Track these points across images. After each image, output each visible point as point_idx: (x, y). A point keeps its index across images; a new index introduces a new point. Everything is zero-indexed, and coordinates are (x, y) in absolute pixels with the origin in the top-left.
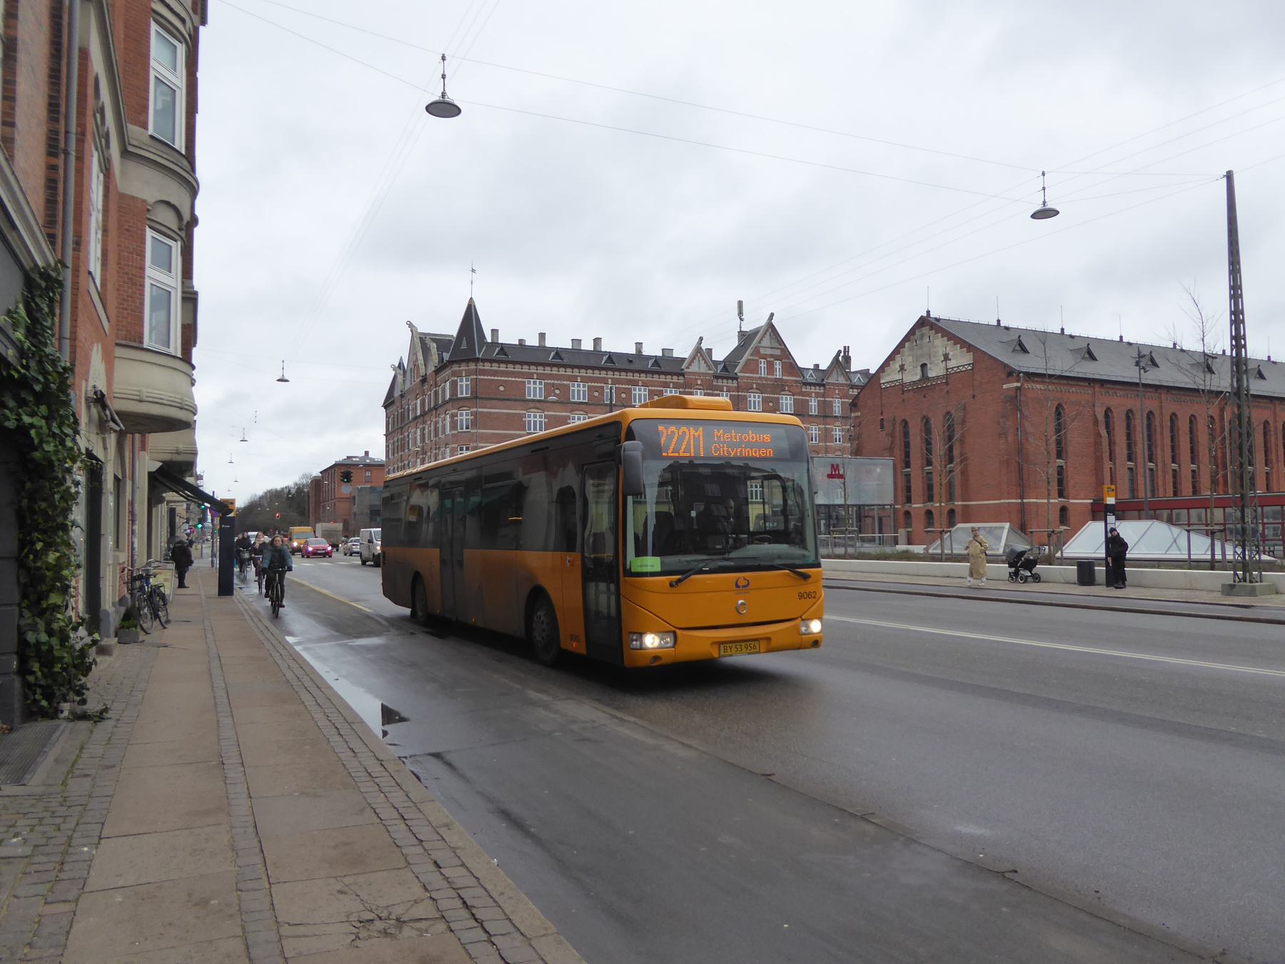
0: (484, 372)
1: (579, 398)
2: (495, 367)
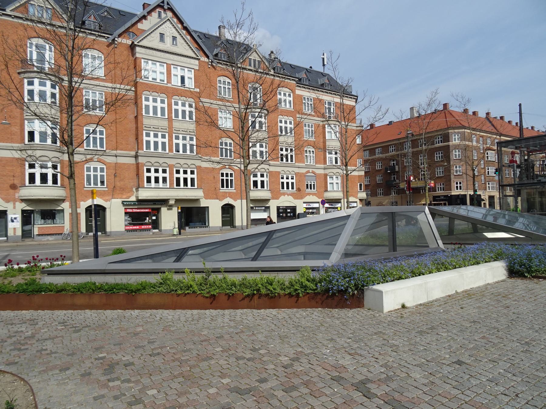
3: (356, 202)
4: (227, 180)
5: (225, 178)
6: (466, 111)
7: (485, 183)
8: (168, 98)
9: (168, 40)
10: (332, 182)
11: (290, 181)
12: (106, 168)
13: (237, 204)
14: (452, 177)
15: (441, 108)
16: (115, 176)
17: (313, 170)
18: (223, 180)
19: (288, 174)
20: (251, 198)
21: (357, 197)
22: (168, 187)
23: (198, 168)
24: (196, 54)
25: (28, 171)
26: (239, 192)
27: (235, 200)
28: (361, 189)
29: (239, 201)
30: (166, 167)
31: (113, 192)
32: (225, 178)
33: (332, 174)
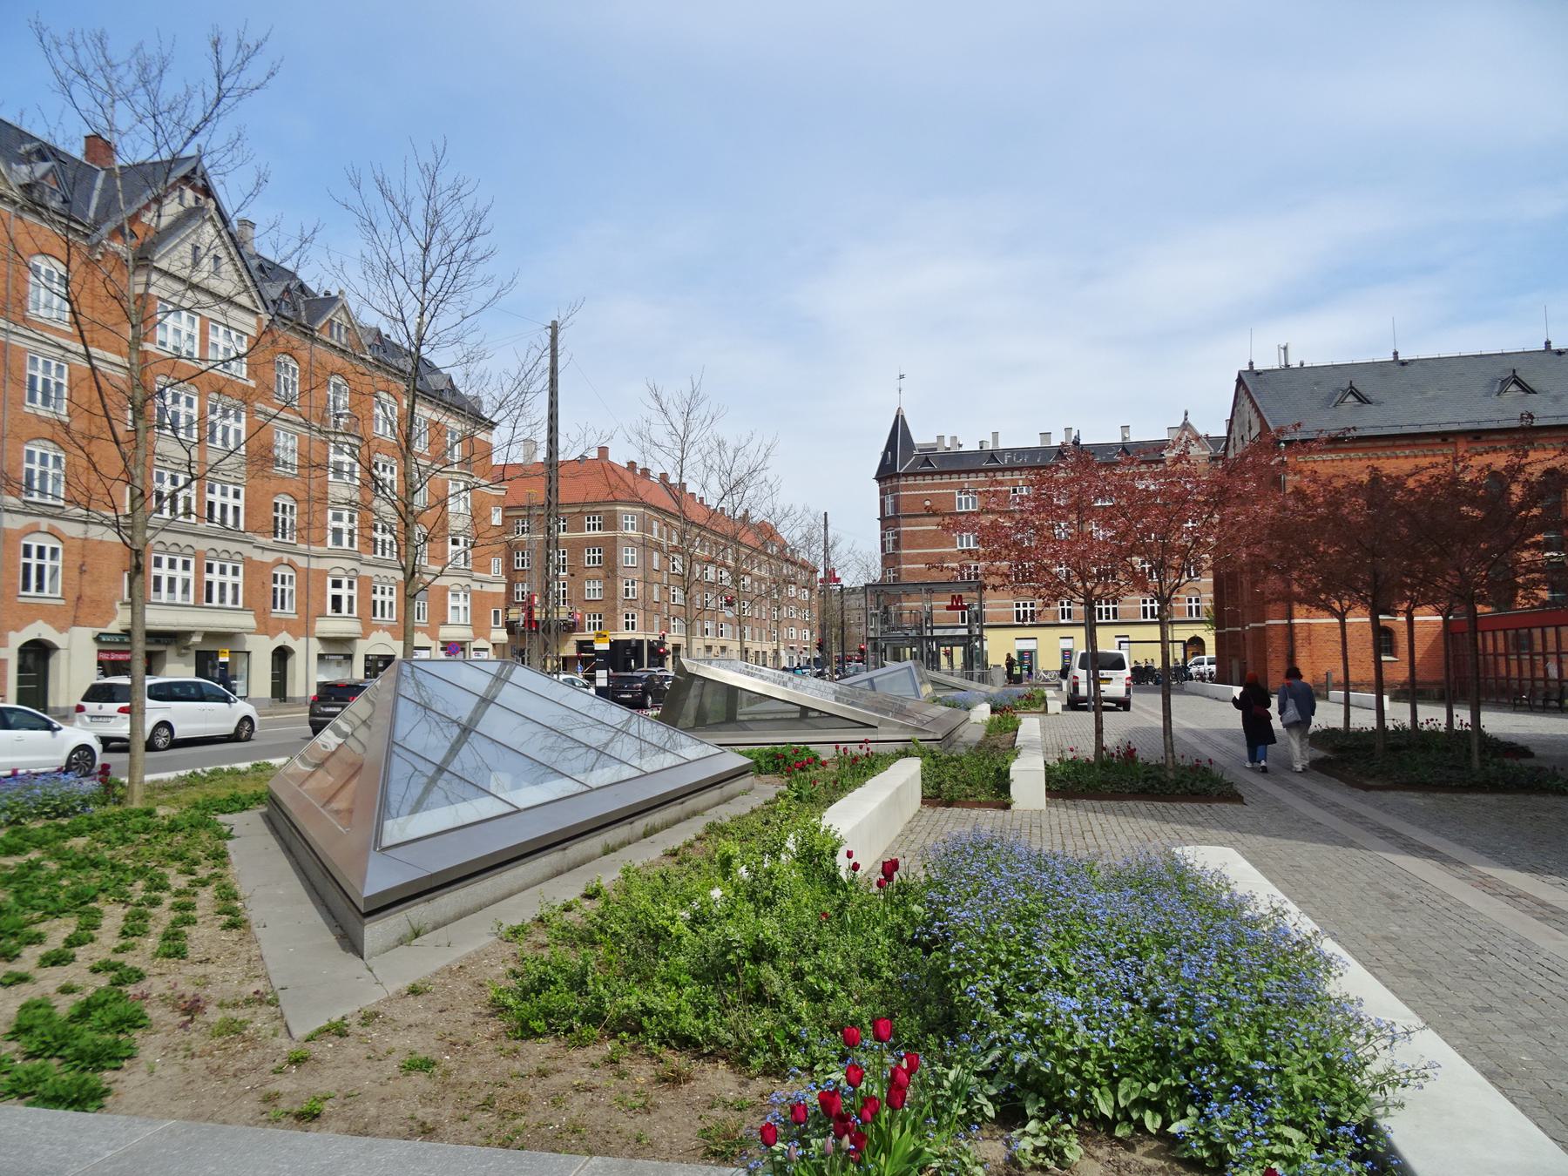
0: (907, 488)
1: (967, 507)
2: (920, 481)
3: (486, 650)
4: (40, 569)
5: (279, 586)
6: (632, 465)
7: (668, 619)
8: (199, 395)
9: (207, 264)
10: (455, 604)
11: (229, 579)
12: (64, 550)
13: (298, 645)
14: (619, 603)
15: (594, 454)
16: (82, 572)
17: (53, 522)
18: (27, 567)
19: (174, 554)
20: (148, 627)
21: (488, 639)
22: (192, 602)
23: (248, 561)
24: (254, 302)
25: (331, 591)
26: (304, 619)
27: (296, 638)
28: (496, 622)
29: (303, 640)
30: (191, 556)
31: (77, 610)
32: (34, 561)
33: (458, 588)
